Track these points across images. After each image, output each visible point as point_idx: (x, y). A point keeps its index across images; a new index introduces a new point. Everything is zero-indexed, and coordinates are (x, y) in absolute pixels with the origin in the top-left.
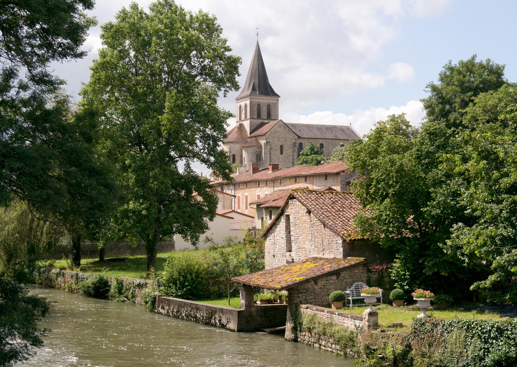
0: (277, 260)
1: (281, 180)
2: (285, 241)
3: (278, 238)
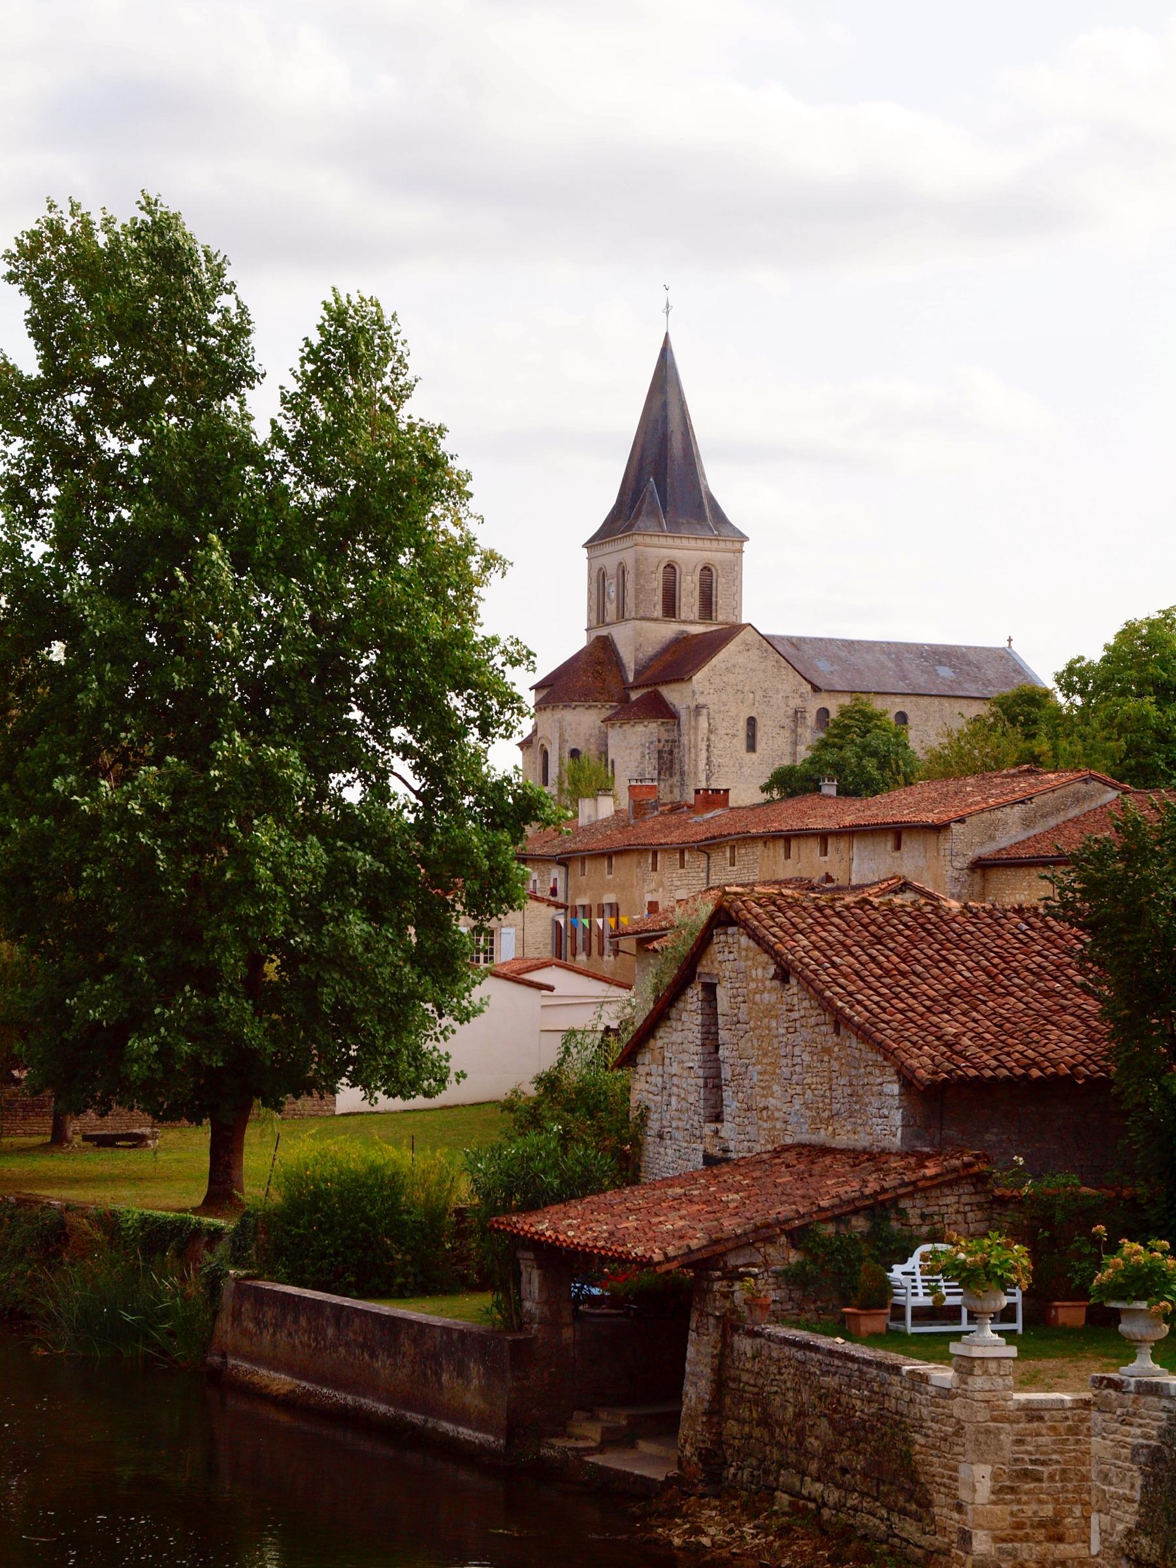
0: (670, 1151)
2: (701, 1082)
3: (675, 1069)
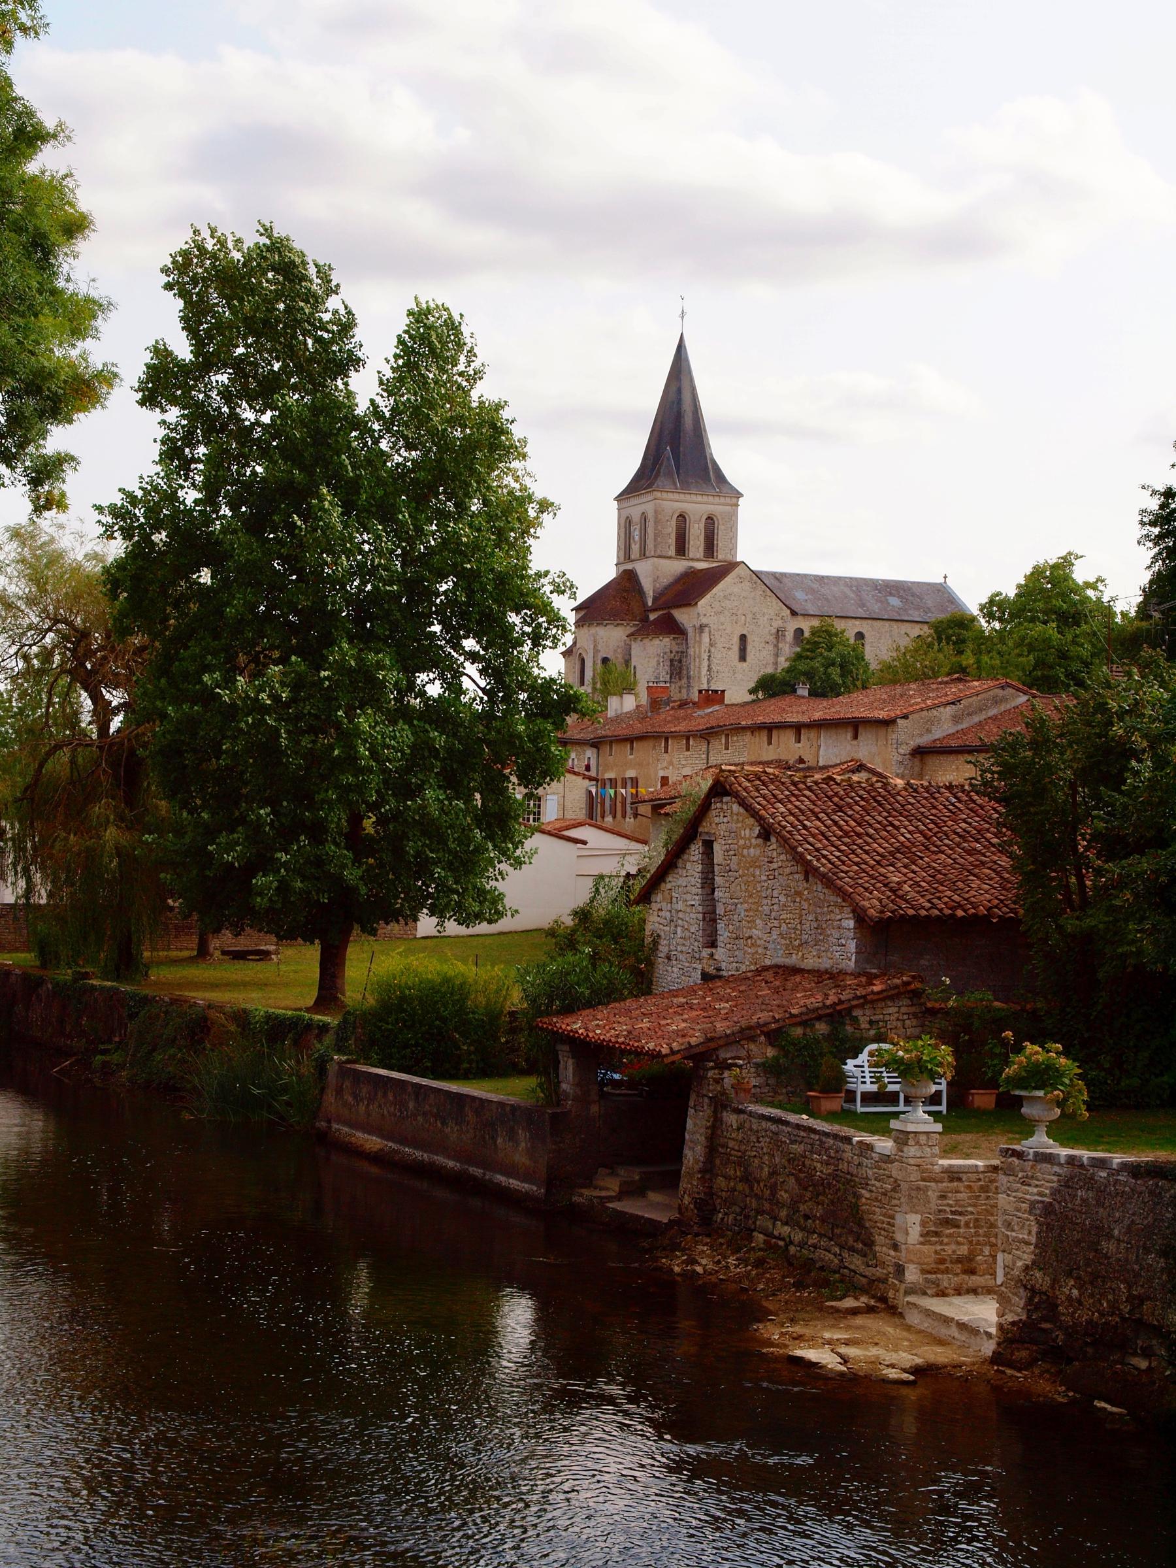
1: (727, 736)
2: (700, 916)
3: (680, 906)
